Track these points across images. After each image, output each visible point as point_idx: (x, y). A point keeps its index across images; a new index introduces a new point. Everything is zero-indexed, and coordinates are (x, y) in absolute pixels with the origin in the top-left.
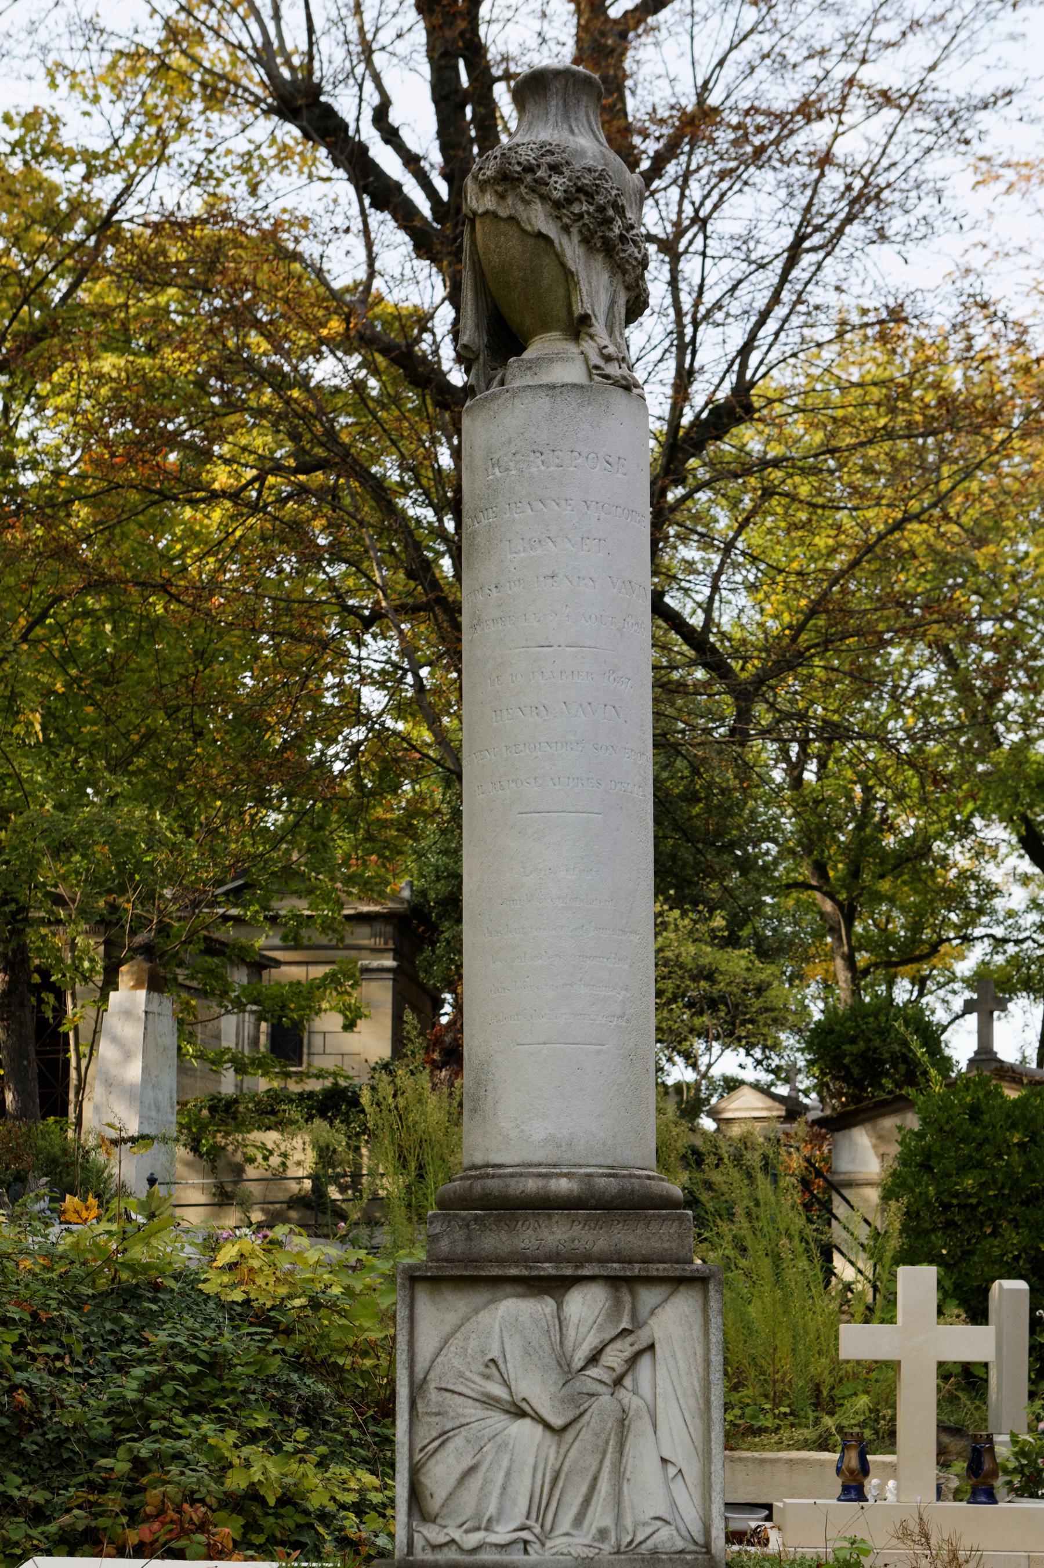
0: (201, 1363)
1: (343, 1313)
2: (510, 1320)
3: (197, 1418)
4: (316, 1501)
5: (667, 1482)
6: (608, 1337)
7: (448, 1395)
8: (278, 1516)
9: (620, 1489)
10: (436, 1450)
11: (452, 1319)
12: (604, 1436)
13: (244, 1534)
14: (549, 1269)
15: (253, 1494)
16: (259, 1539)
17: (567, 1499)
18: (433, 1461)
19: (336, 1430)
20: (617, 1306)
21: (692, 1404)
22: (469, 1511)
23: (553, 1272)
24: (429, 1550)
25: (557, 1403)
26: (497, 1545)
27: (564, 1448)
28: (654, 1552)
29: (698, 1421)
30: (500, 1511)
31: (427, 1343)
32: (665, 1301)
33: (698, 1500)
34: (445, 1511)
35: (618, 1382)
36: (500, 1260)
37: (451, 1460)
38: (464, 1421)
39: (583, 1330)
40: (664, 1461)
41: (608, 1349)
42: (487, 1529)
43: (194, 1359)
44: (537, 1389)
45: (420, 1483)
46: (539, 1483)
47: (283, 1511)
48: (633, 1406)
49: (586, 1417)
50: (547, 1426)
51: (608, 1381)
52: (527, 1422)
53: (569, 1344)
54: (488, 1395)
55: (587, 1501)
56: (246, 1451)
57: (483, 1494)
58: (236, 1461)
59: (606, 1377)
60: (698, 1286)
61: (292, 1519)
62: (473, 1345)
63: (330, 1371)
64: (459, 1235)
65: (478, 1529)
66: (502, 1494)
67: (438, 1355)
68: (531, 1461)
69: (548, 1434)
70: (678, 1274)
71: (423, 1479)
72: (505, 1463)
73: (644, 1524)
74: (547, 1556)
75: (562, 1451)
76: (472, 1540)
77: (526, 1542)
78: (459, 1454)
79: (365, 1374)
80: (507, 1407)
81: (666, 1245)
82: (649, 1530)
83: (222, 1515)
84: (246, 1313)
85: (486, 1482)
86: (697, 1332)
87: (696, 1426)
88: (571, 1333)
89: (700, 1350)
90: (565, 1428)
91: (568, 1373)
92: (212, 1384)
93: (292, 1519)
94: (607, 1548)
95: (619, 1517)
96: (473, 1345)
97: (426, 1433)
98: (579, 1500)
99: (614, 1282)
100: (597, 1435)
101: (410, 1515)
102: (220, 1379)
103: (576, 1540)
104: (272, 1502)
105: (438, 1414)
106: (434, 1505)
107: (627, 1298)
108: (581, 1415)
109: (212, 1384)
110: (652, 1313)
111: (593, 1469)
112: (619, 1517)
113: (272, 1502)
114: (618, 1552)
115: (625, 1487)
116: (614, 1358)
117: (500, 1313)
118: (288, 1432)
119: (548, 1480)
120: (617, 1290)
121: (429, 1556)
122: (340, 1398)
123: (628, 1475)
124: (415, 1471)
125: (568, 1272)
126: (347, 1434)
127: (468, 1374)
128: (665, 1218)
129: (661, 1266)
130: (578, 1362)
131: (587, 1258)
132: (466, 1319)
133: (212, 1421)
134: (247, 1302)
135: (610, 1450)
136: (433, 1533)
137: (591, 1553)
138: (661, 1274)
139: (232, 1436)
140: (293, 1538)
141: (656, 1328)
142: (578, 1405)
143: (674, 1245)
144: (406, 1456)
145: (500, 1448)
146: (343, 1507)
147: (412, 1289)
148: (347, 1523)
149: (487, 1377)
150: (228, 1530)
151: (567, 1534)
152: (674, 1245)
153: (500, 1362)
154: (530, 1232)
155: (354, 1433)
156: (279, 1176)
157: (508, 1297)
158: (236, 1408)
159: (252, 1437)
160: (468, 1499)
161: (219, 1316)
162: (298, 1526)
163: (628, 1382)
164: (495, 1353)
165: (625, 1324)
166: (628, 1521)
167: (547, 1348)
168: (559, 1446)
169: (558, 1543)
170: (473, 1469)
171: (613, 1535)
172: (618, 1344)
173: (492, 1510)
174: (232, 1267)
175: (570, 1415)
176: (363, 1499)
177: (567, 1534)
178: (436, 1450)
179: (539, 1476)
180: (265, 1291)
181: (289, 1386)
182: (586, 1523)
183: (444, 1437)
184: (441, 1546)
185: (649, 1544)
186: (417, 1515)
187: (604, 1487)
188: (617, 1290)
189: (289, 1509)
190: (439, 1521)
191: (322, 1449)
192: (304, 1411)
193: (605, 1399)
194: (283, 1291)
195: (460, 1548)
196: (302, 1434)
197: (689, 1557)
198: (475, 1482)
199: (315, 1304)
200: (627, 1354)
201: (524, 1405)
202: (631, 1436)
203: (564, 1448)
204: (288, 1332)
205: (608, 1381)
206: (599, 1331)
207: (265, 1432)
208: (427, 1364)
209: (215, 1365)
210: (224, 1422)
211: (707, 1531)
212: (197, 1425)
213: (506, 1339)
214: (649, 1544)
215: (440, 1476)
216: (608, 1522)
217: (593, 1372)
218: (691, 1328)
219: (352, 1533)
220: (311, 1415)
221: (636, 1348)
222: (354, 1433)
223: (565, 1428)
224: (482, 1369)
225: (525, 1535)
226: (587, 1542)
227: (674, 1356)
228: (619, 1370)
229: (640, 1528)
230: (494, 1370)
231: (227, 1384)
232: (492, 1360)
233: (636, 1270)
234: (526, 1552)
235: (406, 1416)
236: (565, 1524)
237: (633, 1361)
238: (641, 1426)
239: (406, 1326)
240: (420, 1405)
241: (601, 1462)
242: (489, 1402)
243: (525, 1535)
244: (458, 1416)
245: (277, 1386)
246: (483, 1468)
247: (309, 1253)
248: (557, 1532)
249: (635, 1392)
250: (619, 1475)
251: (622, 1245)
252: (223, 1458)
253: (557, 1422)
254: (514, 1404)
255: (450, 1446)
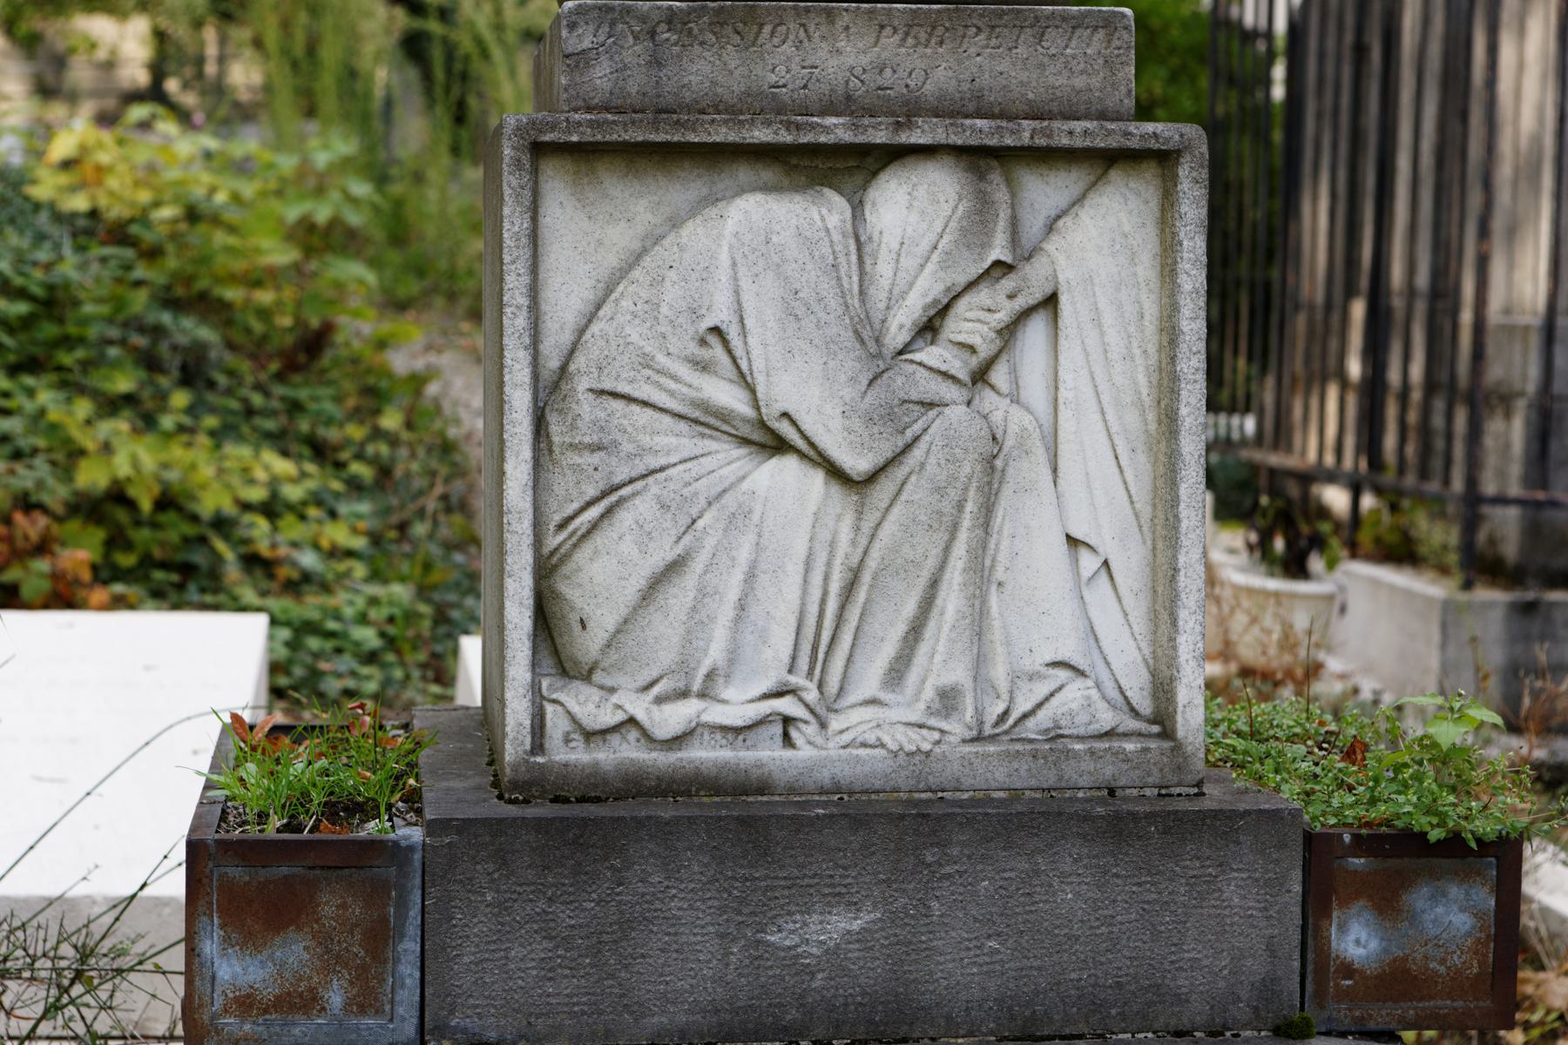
0: (31, 298)
1: (232, 229)
2: (754, 239)
3: (29, 380)
4: (212, 502)
5: (1079, 586)
6: (962, 279)
7: (618, 405)
8: (155, 525)
9: (984, 601)
10: (594, 526)
11: (620, 237)
12: (954, 494)
13: (107, 555)
14: (837, 130)
15: (118, 495)
16: (127, 560)
17: (874, 627)
19: (229, 392)
20: (982, 209)
21: (1134, 423)
22: (666, 657)
23: (847, 136)
24: (578, 741)
25: (857, 424)
26: (725, 729)
28: (1055, 736)
29: (1142, 458)
30: (733, 656)
31: (566, 297)
32: (1079, 200)
33: (1140, 624)
34: (613, 656)
35: (980, 376)
36: (731, 111)
37: (628, 547)
38: (655, 463)
39: (909, 263)
40: (1072, 541)
41: (962, 306)
42: (702, 695)
43: (22, 294)
44: (812, 390)
45: (557, 596)
46: (815, 594)
47: (163, 518)
48: (1013, 428)
49: (918, 453)
50: (835, 472)
51: (963, 375)
52: (790, 463)
53: (879, 295)
54: (705, 407)
55: (915, 632)
56: (105, 428)
57: (697, 621)
58: (90, 445)
59: (959, 366)
60: (1150, 170)
61: (176, 530)
62: (672, 295)
63: (205, 305)
64: (634, 53)
65: (684, 694)
66: (738, 620)
67: (591, 318)
68: (800, 548)
69: (836, 490)
70: (1113, 142)
71: (564, 588)
72: (744, 554)
73: (1032, 677)
74: (833, 749)
75: (867, 527)
76: (671, 718)
77: (787, 721)
78: (645, 535)
79: (264, 314)
80: (745, 431)
81: (1079, 82)
82: (1042, 689)
83: (74, 525)
84: (92, 229)
85: (702, 593)
86: (1146, 268)
87: (1140, 471)
88: (883, 269)
89: (1151, 309)
90: (872, 478)
91: (880, 359)
92: (49, 330)
93: (176, 530)
94: (956, 728)
95: (980, 663)
96: (672, 295)
97: (572, 487)
98: (901, 628)
99: (978, 159)
100: (939, 490)
102: (61, 321)
103: (894, 714)
104: (146, 505)
105: (596, 448)
106: (588, 645)
107: (1001, 195)
108: (908, 447)
109: (49, 330)
110: (1050, 227)
111: (931, 563)
112: (980, 663)
113: (146, 505)
114: (978, 739)
115: (994, 600)
116: (972, 325)
117: (730, 225)
118: (162, 397)
119: (835, 587)
120: (982, 177)
121: (579, 755)
122: (231, 346)
123: (1000, 574)
124: (546, 570)
125: (880, 137)
126: (245, 401)
127: (661, 359)
128: (1077, 24)
129: (1078, 126)
130: (897, 334)
131: (909, 110)
132: (654, 239)
133: (51, 386)
134: (94, 214)
135: (966, 522)
136: (585, 704)
137: (925, 740)
138: (1079, 143)
139: (83, 408)
140: (180, 557)
141: (1061, 261)
142: (900, 424)
143: (1095, 82)
144: (528, 540)
145: (736, 520)
146: (246, 507)
147: (535, 171)
148: (256, 533)
149: (703, 367)
150: (79, 554)
152: (1095, 82)
154: (788, 49)
155: (257, 400)
156: (110, 65)
157: (741, 191)
158: (86, 365)
159: (111, 405)
160: (663, 634)
161: (54, 230)
162: (186, 540)
163: (999, 376)
164: (721, 314)
165: (999, 251)
166: (999, 674)
167: (834, 303)
168: (859, 514)
169: (853, 721)
170: (674, 568)
171: (969, 701)
172: (983, 296)
173: (715, 654)
174: (67, 165)
175: (886, 450)
176: (275, 495)
178: (594, 526)
180: (119, 194)
181: (157, 331)
182: (913, 677)
183: (612, 497)
184: (604, 732)
185: (1043, 718)
186: (547, 663)
187: (952, 600)
188: (982, 177)
189: (169, 517)
190: (598, 677)
191: (211, 421)
192: (184, 368)
193: (956, 413)
194: (144, 196)
195: (645, 734)
196: (180, 399)
197: (1130, 746)
198: (679, 596)
199: (193, 215)
202: (1007, 492)
204: (153, 254)
205: (963, 375)
206: (944, 265)
207: (129, 399)
208: (567, 338)
209: (54, 302)
210: (70, 386)
211: (1163, 689)
212: (31, 393)
213: (745, 283)
214: (1043, 718)
215: (602, 582)
216: (958, 674)
217: (931, 355)
218: (1133, 261)
219: (263, 548)
220: (193, 373)
221: (1021, 302)
222: (257, 400)
223: (872, 478)
224: (693, 348)
225: (786, 705)
226: (915, 716)
227: (1097, 321)
228: (985, 351)
229: (1024, 685)
230: (718, 351)
231: (72, 330)
232: (716, 330)
233: (1025, 133)
234: (787, 740)
235: (527, 453)
236: (869, 681)
237: (1009, 332)
238: (1029, 469)
239: (526, 253)
240: (556, 428)
241: (947, 549)
242: (707, 420)
243: (786, 705)
244: (642, 451)
245: (142, 329)
246: (697, 566)
247: (179, 148)
248: (853, 697)
249: (1015, 399)
250: (981, 574)
251: (985, 80)
252: (68, 441)
253: (857, 463)
254: (762, 424)
255: (625, 517)
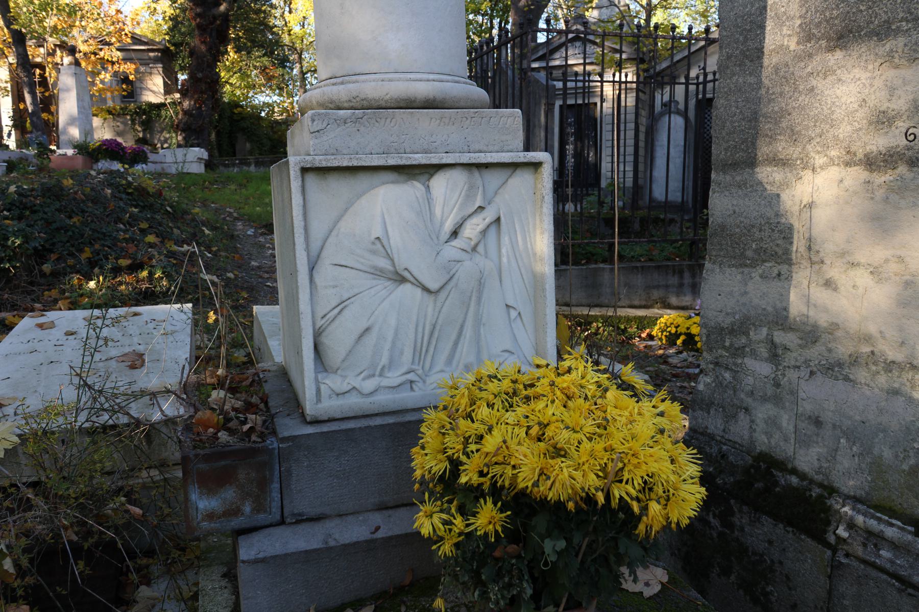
9: (479, 331)
18: (333, 326)
20: (472, 187)
27: (439, 304)
38: (356, 291)
42: (381, 375)
50: (425, 289)
52: (407, 287)
54: (375, 268)
55: (456, 344)
60: (532, 170)
69: (425, 294)
76: (368, 385)
77: (411, 382)
80: (390, 276)
101: (317, 372)
107: (479, 182)
123: (484, 320)
144: (310, 323)
149: (374, 252)
151: (442, 371)
153: (385, 242)
163: (480, 248)
172: (475, 220)
177: (442, 371)
179: (420, 329)
187: (468, 332)
200: (481, 227)
201: (406, 274)
203: (439, 304)
216: (472, 359)
217: (455, 243)
230: (379, 246)
243: (411, 376)
248: (434, 371)
253: (433, 286)
255: (346, 312)
